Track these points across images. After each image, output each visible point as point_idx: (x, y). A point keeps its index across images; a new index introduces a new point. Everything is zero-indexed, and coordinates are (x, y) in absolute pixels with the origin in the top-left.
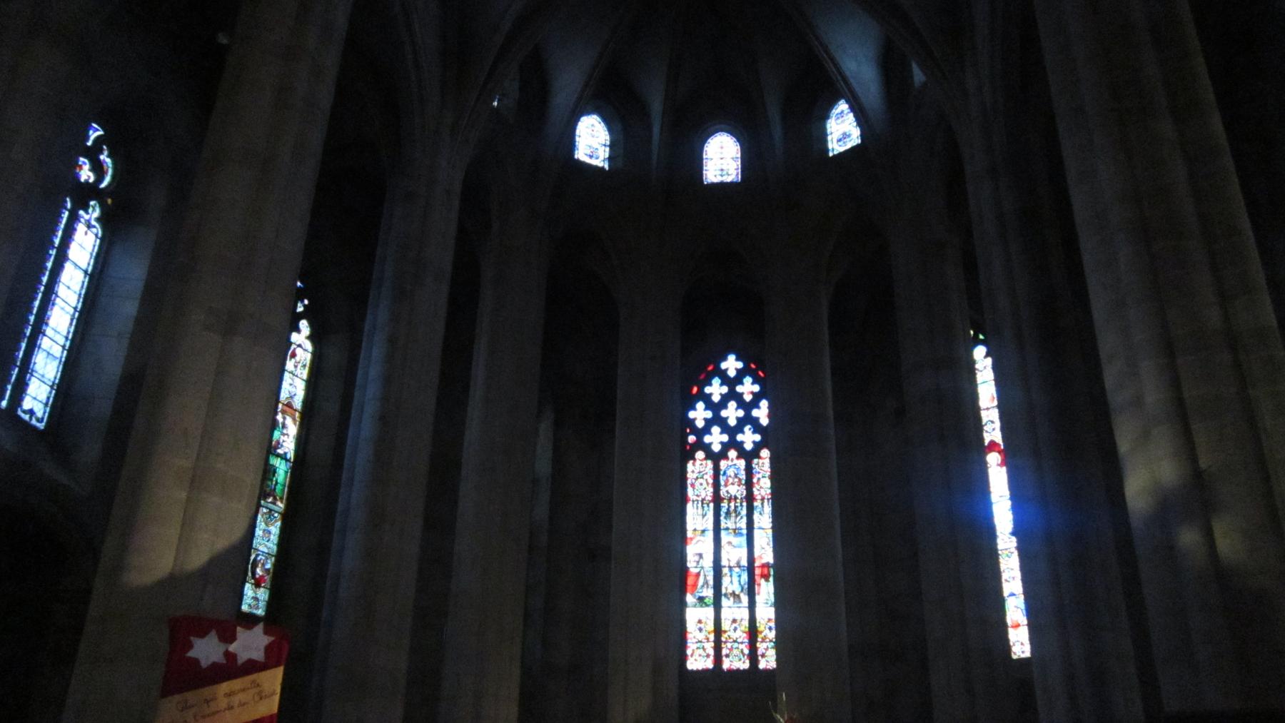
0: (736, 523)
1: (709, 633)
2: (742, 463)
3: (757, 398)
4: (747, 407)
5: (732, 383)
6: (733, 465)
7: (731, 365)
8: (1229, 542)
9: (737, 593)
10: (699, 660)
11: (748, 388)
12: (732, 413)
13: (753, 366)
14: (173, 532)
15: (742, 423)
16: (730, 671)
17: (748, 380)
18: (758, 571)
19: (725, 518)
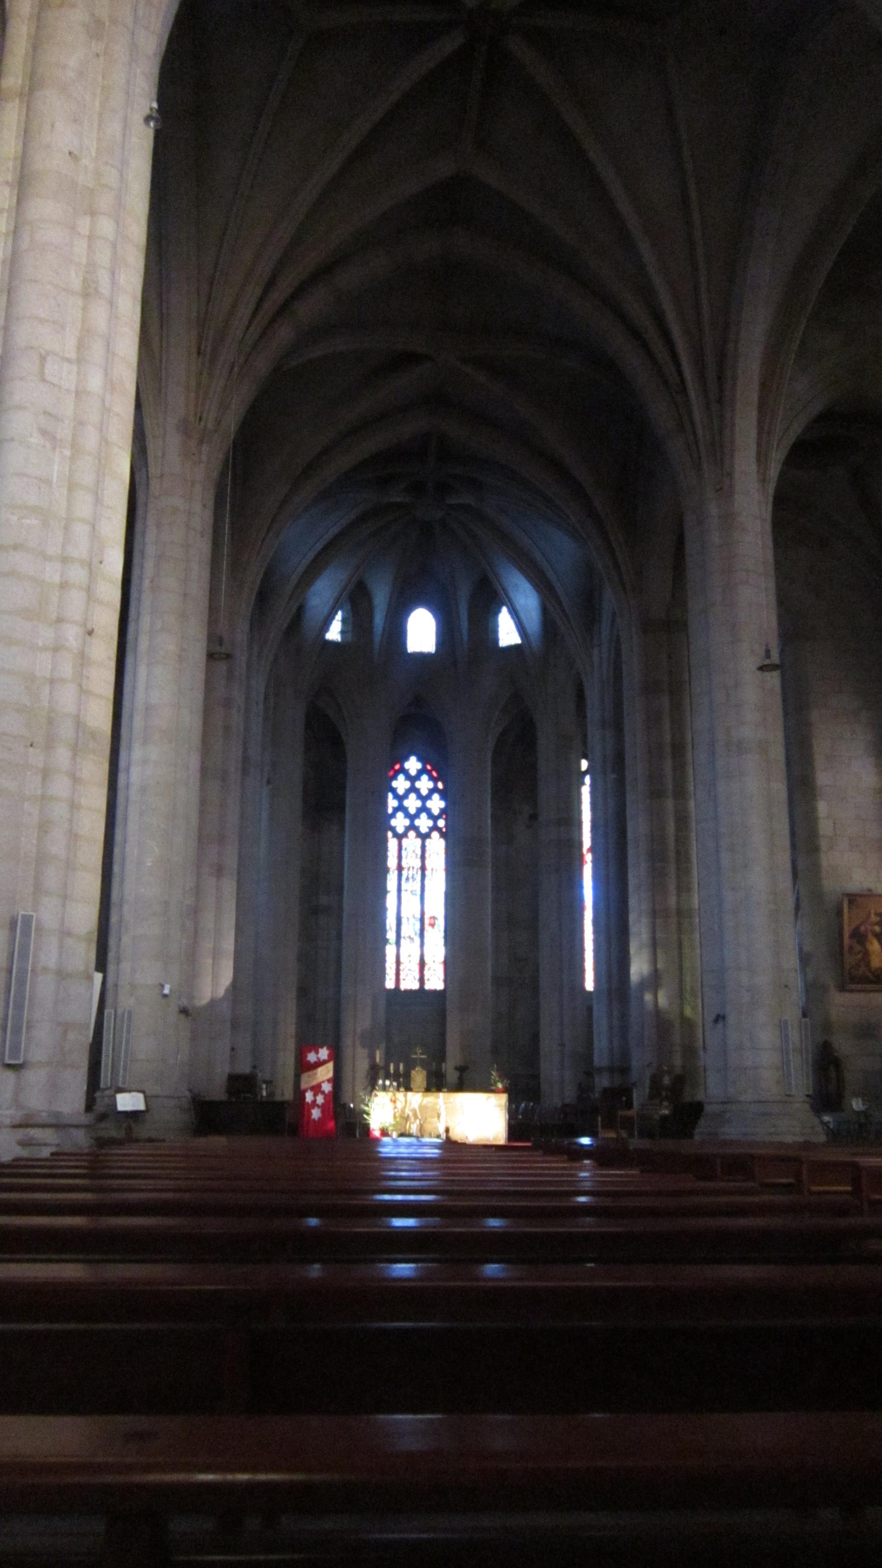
0: (413, 886)
1: (392, 964)
2: (419, 841)
3: (420, 773)
4: (424, 799)
5: (413, 779)
6: (412, 843)
7: (413, 765)
8: (663, 1000)
9: (412, 937)
10: (390, 984)
11: (425, 784)
12: (412, 803)
13: (429, 767)
14: (209, 979)
15: (420, 811)
16: (406, 991)
17: (425, 778)
18: (427, 922)
19: (405, 882)
